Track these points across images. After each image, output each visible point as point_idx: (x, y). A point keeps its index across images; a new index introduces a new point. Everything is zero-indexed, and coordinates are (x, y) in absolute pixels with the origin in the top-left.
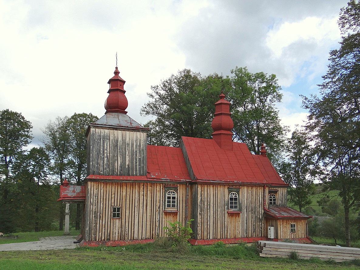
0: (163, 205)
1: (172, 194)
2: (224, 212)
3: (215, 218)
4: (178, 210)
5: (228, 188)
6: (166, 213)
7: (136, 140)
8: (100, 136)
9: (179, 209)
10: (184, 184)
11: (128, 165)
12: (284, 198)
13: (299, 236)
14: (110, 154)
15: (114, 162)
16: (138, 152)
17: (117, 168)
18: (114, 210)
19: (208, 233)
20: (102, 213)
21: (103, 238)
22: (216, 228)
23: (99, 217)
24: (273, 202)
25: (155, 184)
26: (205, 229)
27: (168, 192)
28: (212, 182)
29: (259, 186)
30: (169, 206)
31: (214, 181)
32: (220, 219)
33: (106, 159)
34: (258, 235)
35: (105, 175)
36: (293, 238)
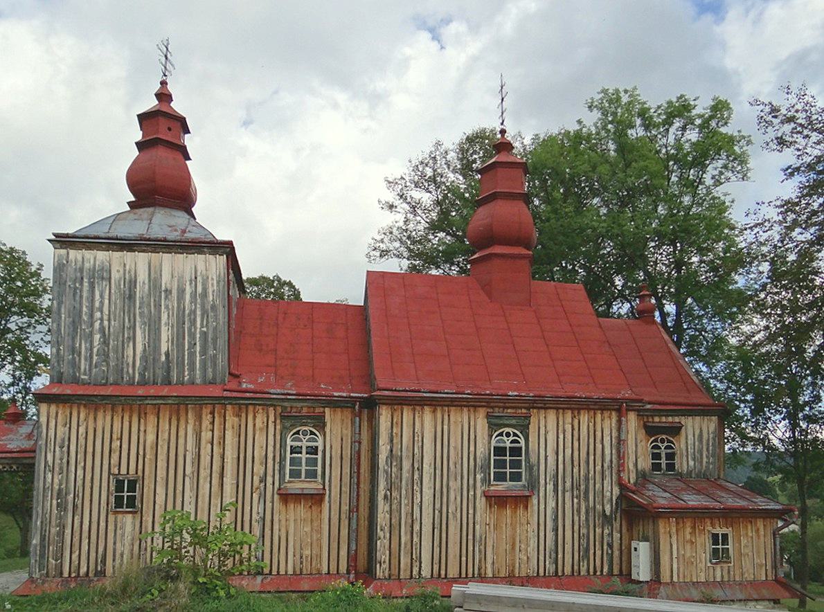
0: (277, 472)
1: (308, 437)
2: (472, 493)
3: (441, 512)
4: (327, 488)
5: (488, 416)
6: (286, 498)
7: (193, 278)
8: (81, 270)
9: (330, 486)
10: (348, 407)
11: (167, 354)
12: (705, 449)
13: (746, 575)
14: (113, 323)
15: (123, 345)
16: (199, 313)
17: (131, 363)
18: (119, 486)
19: (415, 560)
20: (81, 495)
21: (83, 570)
22: (441, 543)
23: (70, 507)
24: (663, 462)
25: (251, 408)
26: (403, 546)
27: (295, 431)
28: (428, 395)
29: (602, 410)
30: (295, 474)
31: (437, 393)
32: (459, 514)
33: (97, 337)
34: (598, 570)
35: (94, 385)
36: (719, 579)
